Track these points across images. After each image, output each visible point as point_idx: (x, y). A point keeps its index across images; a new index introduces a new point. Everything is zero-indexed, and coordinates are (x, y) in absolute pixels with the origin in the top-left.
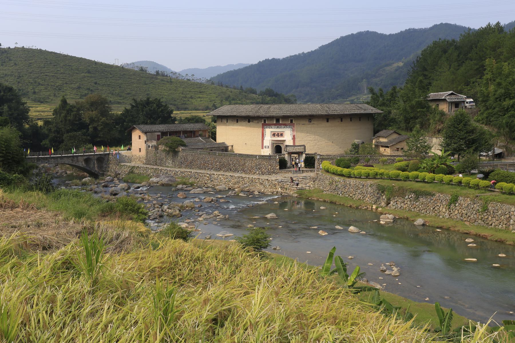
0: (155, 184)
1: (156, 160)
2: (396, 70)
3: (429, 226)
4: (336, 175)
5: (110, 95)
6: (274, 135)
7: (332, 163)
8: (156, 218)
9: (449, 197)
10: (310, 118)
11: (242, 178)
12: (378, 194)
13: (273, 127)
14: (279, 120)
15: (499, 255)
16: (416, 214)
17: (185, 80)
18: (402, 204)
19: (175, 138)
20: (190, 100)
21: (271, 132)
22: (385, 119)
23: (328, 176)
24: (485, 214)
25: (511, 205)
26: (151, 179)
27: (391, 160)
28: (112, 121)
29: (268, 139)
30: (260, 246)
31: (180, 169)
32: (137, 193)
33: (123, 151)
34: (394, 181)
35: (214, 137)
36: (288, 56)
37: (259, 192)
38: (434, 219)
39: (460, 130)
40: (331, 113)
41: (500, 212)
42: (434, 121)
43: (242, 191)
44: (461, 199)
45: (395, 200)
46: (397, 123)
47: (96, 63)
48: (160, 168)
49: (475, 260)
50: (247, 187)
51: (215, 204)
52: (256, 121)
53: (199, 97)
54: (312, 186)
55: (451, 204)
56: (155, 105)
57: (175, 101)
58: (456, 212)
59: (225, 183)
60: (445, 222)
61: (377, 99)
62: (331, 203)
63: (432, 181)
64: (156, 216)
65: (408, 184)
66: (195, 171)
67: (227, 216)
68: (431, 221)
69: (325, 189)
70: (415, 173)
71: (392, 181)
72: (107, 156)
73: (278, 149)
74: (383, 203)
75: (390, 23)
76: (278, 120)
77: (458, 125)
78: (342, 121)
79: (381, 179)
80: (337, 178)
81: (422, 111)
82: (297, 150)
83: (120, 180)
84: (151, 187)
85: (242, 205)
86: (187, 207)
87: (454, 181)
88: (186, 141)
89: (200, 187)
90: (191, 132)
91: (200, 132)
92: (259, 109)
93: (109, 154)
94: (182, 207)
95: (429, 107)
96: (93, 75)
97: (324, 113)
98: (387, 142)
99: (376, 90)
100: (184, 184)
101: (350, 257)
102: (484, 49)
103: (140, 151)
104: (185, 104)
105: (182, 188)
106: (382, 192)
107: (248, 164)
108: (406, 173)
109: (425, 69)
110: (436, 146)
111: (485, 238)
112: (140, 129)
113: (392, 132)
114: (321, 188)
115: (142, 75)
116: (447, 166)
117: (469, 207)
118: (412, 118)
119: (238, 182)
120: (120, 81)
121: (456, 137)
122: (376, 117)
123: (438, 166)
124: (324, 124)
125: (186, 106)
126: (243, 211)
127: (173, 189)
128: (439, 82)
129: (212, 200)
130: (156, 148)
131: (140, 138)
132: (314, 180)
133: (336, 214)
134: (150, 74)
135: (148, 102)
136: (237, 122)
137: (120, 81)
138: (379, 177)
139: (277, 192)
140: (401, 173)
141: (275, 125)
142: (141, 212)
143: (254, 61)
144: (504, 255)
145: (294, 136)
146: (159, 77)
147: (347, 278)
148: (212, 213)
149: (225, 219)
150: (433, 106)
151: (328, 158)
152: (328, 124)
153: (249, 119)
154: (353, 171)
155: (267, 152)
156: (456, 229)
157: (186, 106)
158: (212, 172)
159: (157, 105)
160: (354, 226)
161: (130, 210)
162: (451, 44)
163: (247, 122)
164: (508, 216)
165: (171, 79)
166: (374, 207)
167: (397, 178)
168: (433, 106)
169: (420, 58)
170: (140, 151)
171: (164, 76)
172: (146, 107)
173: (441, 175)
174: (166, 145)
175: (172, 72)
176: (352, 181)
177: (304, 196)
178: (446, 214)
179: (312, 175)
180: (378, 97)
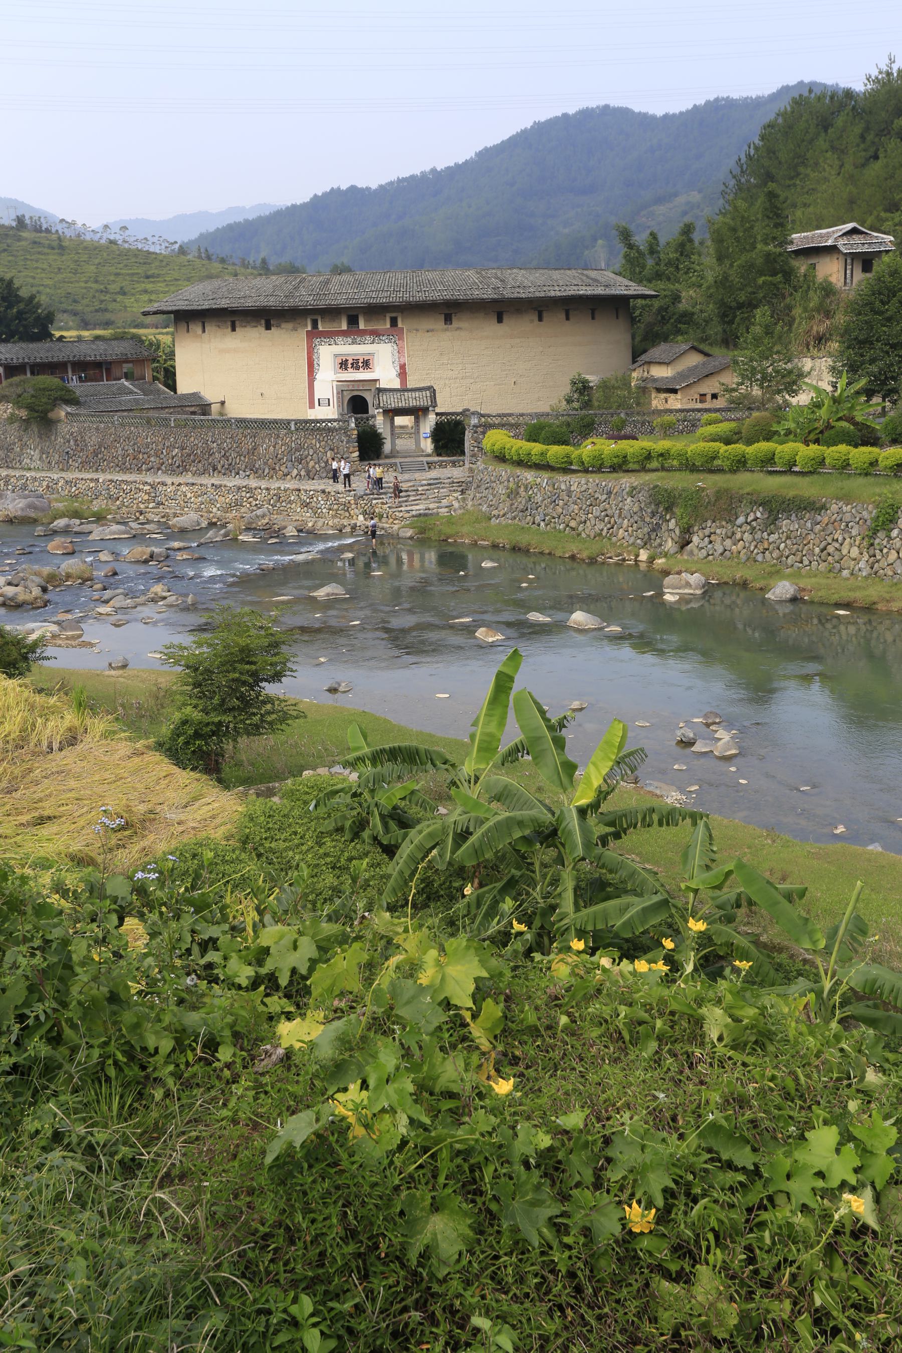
3: (812, 602)
4: (530, 467)
6: (344, 365)
7: (516, 436)
9: (869, 513)
10: (449, 310)
11: (250, 490)
12: (653, 514)
13: (339, 340)
14: (355, 318)
16: (768, 569)
17: (103, 241)
18: (728, 542)
20: (119, 298)
21: (336, 356)
22: (663, 317)
23: (504, 471)
27: (688, 423)
29: (328, 380)
30: (254, 674)
31: (64, 475)
34: (701, 476)
36: (393, 177)
37: (300, 531)
38: (824, 581)
39: (889, 319)
40: (508, 294)
42: (805, 310)
43: (248, 529)
45: (707, 532)
46: (698, 325)
50: (263, 516)
51: (159, 565)
52: (290, 325)
53: (146, 291)
54: (456, 505)
55: (875, 532)
57: (75, 301)
59: (198, 510)
60: (859, 588)
61: (641, 261)
62: (516, 549)
63: (817, 467)
65: (744, 481)
66: (109, 477)
67: (190, 600)
68: (818, 585)
69: (495, 512)
70: (763, 446)
71: (695, 476)
73: (357, 404)
74: (670, 543)
75: (664, 88)
76: (353, 321)
77: (883, 303)
78: (540, 319)
79: (663, 469)
80: (529, 476)
81: (772, 283)
82: (411, 400)
85: (246, 566)
86: (68, 576)
87: (882, 464)
90: (98, 365)
91: (126, 367)
92: (296, 288)
97: (489, 294)
98: (673, 378)
99: (641, 239)
100: (76, 514)
104: (106, 310)
105: (68, 526)
106: (668, 509)
107: (266, 447)
108: (739, 447)
109: (769, 177)
110: (820, 376)
113: (685, 347)
114: (484, 508)
116: (856, 424)
118: (740, 306)
119: (238, 504)
122: (637, 313)
123: (829, 427)
124: (490, 328)
125: (108, 316)
126: (245, 582)
128: (811, 209)
129: (152, 556)
132: (463, 487)
133: (530, 582)
136: (234, 329)
138: (655, 464)
139: (354, 527)
140: (723, 448)
143: (297, 192)
145: (403, 367)
146: (24, 234)
147: (571, 776)
148: (144, 593)
150: (801, 266)
151: (505, 422)
153: (267, 317)
154: (577, 452)
155: (329, 413)
157: (108, 316)
158: (160, 477)
160: (588, 612)
162: (842, 106)
163: (261, 329)
165: (59, 239)
166: (644, 556)
168: (801, 266)
169: (757, 148)
171: (40, 231)
173: (843, 448)
174: (18, 404)
175: (62, 220)
176: (576, 483)
178: (862, 564)
179: (457, 473)
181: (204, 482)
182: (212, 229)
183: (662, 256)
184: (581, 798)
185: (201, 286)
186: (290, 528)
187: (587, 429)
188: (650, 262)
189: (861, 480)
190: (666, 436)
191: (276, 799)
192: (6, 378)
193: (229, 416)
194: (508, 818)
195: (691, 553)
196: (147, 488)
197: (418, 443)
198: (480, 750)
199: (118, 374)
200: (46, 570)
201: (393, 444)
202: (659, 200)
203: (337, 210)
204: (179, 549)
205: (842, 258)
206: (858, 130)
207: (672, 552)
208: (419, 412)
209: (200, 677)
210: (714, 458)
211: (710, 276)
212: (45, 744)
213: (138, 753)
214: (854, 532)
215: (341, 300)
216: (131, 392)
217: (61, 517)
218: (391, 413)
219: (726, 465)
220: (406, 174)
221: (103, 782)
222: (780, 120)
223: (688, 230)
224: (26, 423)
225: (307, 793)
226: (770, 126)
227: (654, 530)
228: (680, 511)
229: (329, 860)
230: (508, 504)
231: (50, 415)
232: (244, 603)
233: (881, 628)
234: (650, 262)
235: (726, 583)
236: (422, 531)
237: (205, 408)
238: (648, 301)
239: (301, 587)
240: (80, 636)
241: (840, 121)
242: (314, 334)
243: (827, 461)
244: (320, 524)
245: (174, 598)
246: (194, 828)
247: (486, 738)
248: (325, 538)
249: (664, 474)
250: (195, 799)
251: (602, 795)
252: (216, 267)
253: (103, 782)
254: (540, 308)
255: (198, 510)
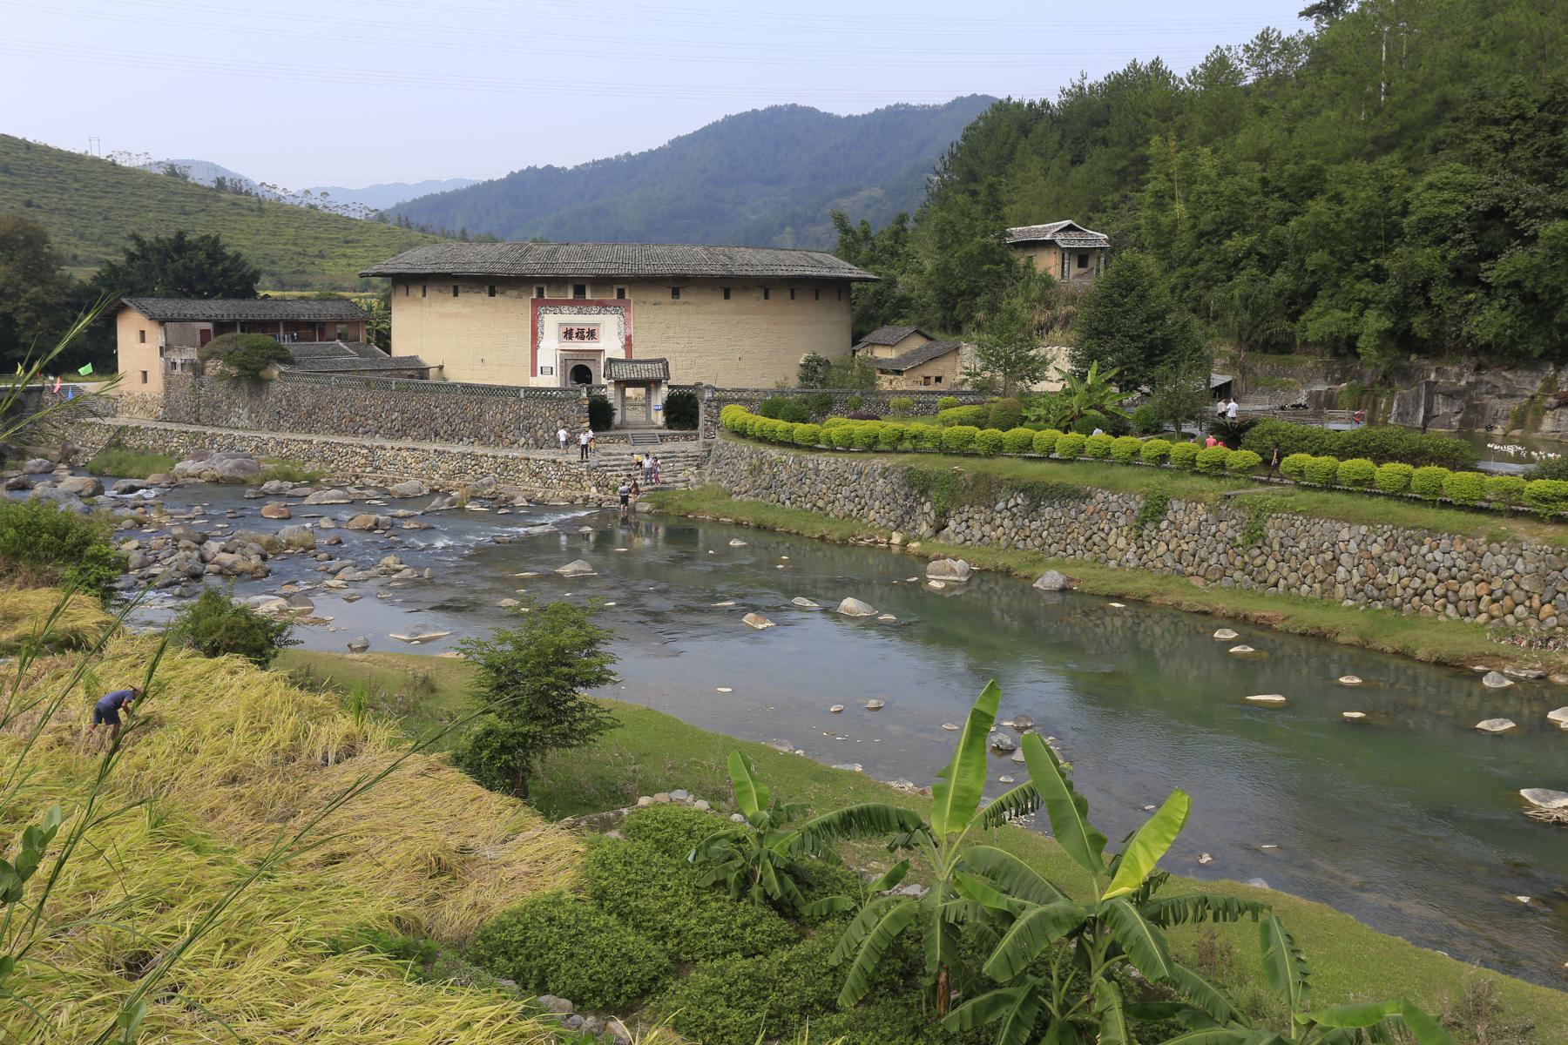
0: (192, 480)
1: (198, 406)
2: (868, 207)
3: (1082, 593)
4: (773, 444)
5: (73, 240)
6: (568, 334)
7: (751, 411)
8: (176, 583)
9: (1138, 503)
10: (677, 285)
11: (475, 457)
12: (907, 497)
13: (565, 309)
15: (1342, 680)
16: (1030, 557)
18: (987, 528)
19: (257, 337)
20: (318, 261)
23: (746, 447)
24: (1256, 552)
25: (1338, 520)
26: (178, 466)
28: (64, 298)
29: (551, 348)
31: (274, 435)
32: (123, 506)
33: (86, 382)
34: (958, 460)
35: (384, 340)
36: (589, 160)
37: (529, 501)
39: (1126, 312)
40: (736, 271)
41: (1303, 545)
42: (1027, 300)
43: (473, 498)
44: (1176, 507)
45: (964, 516)
47: (28, 146)
48: (210, 431)
49: (1278, 698)
50: (489, 485)
51: (386, 535)
52: (515, 293)
53: (345, 256)
54: (693, 479)
56: (202, 255)
57: (273, 262)
58: (1162, 548)
62: (760, 528)
63: (1074, 457)
64: (177, 574)
65: (1005, 466)
67: (426, 573)
68: (1091, 578)
69: (736, 489)
71: (949, 460)
72: (35, 396)
73: (581, 374)
75: (849, 90)
76: (580, 291)
78: (766, 297)
79: (915, 450)
80: (774, 453)
83: (74, 470)
84: (175, 488)
85: (481, 537)
86: (289, 544)
88: (292, 347)
89: (339, 488)
90: (311, 325)
91: (340, 328)
93: (41, 390)
94: (271, 545)
95: (1010, 263)
96: (19, 180)
97: (718, 271)
98: (898, 360)
99: (854, 223)
100: (288, 477)
101: (873, 703)
102: (1142, 117)
103: (145, 380)
105: (280, 489)
106: (922, 492)
110: (1058, 365)
111: (1264, 625)
112: (144, 311)
113: (908, 330)
114: (724, 484)
115: (172, 187)
116: (1106, 413)
117: (1204, 532)
118: (961, 293)
119: (462, 472)
120: (105, 203)
121: (1119, 331)
123: (1082, 415)
124: (717, 304)
125: (305, 278)
126: (482, 555)
127: (250, 492)
130: (197, 369)
131: (143, 340)
132: (700, 462)
134: (196, 185)
135: (179, 245)
136: (456, 295)
137: (105, 203)
138: (907, 445)
139: (586, 499)
140: (979, 433)
141: (570, 303)
142: (95, 558)
143: (498, 171)
144: (1357, 681)
145: (628, 338)
149: (419, 583)
152: (729, 305)
153: (492, 284)
156: (1169, 600)
158: (378, 441)
159: (209, 256)
161: (47, 548)
163: (485, 296)
164: (1329, 556)
165: (259, 201)
166: (896, 538)
167: (963, 450)
168: (1021, 258)
170: (145, 380)
172: (174, 261)
173: (1434, 469)
174: (229, 361)
176: (825, 461)
177: (669, 509)
178: (1130, 555)
179: (692, 447)
180: (858, 241)
181: (427, 447)
182: (408, 200)
183: (877, 243)
184: (1121, 885)
185: (423, 251)
186: (520, 498)
187: (824, 408)
188: (865, 250)
189: (1125, 470)
190: (903, 418)
191: (614, 834)
192: (216, 334)
193: (451, 381)
194: (1041, 915)
195: (947, 538)
196: (364, 451)
197: (648, 415)
198: (954, 808)
199: (332, 335)
200: (265, 538)
201: (623, 415)
202: (844, 193)
203: (532, 189)
204: (404, 517)
205: (1059, 253)
206: (1056, 136)
207: (927, 535)
208: (650, 384)
209: (503, 679)
210: (969, 442)
211: (928, 266)
212: (319, 754)
213: (433, 769)
214: (1121, 522)
215: (569, 270)
216: (347, 354)
217: (271, 479)
218: (622, 384)
219: (981, 449)
220: (601, 157)
221: (397, 806)
222: (981, 124)
223: (902, 219)
224: (237, 380)
225: (658, 830)
226: (972, 128)
227: (907, 513)
228: (935, 493)
229: (717, 926)
230: (750, 480)
231: (262, 373)
232: (484, 579)
233: (1149, 622)
234: (865, 250)
235: (988, 570)
236: (661, 505)
237: (423, 372)
238: (863, 285)
239: (542, 562)
240: (310, 611)
241: (1040, 128)
242: (539, 303)
243: (1088, 449)
244: (550, 495)
245: (409, 571)
246: (526, 874)
247: (960, 794)
248: (556, 509)
249: (916, 456)
250: (517, 832)
251: (1152, 882)
252: (416, 236)
253: (397, 806)
254: (766, 286)
255: (419, 476)
